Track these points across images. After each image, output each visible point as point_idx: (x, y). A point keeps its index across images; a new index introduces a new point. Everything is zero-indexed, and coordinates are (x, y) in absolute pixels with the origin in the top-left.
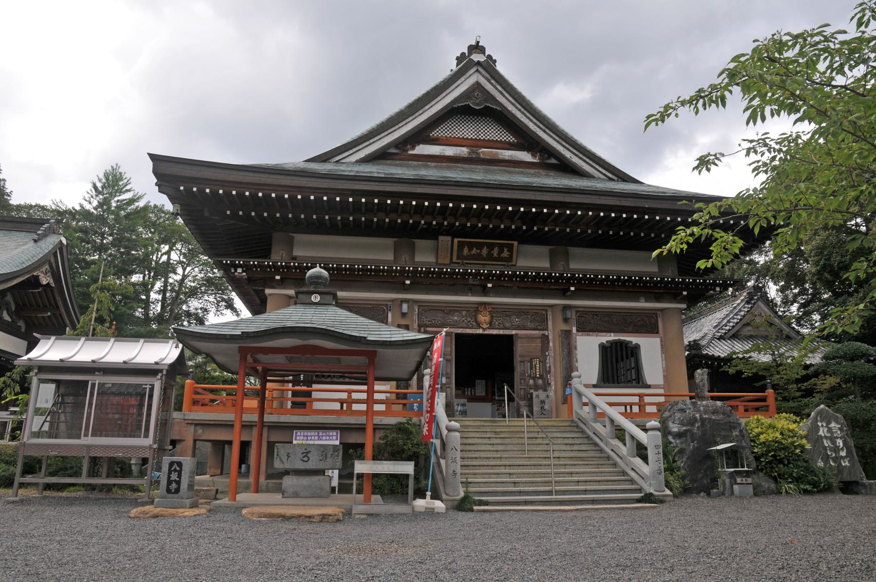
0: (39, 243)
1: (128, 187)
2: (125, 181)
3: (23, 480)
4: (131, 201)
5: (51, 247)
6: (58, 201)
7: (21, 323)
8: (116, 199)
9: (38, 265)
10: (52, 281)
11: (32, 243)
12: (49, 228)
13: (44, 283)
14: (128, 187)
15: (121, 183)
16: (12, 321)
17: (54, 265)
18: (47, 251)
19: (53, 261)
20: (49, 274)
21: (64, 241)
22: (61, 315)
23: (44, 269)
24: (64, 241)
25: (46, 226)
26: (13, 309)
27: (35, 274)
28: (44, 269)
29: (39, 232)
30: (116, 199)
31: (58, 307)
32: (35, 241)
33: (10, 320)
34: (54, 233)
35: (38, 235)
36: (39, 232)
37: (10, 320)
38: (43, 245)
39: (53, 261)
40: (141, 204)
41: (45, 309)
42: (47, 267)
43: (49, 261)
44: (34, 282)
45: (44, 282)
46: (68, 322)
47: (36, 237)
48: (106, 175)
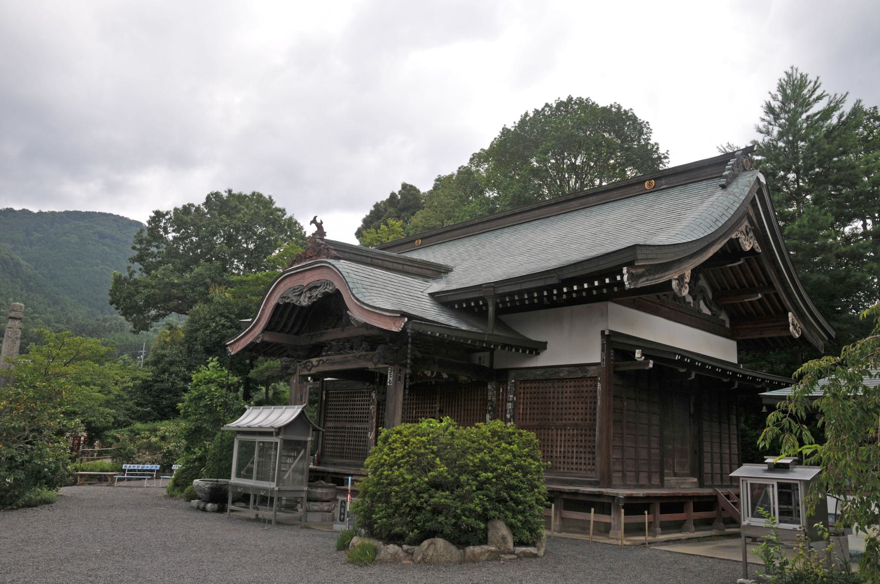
0: (730, 189)
1: (818, 93)
2: (812, 84)
3: (233, 507)
4: (827, 114)
5: (747, 189)
6: (725, 145)
7: (723, 316)
8: (804, 116)
9: (733, 224)
10: (757, 245)
11: (719, 193)
12: (737, 164)
13: (748, 249)
14: (818, 93)
15: (805, 92)
16: (713, 315)
17: (754, 219)
18: (743, 198)
19: (752, 213)
20: (751, 234)
21: (763, 180)
22: (777, 295)
23: (743, 228)
24: (763, 180)
25: (732, 161)
26: (711, 297)
27: (733, 236)
28: (743, 228)
29: (726, 173)
30: (804, 116)
31: (771, 284)
32: (723, 187)
33: (709, 313)
34: (745, 170)
35: (726, 177)
36: (726, 173)
37: (709, 313)
38: (736, 190)
39: (752, 213)
40: (847, 108)
41: (753, 291)
42: (746, 223)
43: (751, 213)
44: (733, 250)
45: (748, 248)
46: (788, 304)
47: (723, 181)
48: (782, 88)
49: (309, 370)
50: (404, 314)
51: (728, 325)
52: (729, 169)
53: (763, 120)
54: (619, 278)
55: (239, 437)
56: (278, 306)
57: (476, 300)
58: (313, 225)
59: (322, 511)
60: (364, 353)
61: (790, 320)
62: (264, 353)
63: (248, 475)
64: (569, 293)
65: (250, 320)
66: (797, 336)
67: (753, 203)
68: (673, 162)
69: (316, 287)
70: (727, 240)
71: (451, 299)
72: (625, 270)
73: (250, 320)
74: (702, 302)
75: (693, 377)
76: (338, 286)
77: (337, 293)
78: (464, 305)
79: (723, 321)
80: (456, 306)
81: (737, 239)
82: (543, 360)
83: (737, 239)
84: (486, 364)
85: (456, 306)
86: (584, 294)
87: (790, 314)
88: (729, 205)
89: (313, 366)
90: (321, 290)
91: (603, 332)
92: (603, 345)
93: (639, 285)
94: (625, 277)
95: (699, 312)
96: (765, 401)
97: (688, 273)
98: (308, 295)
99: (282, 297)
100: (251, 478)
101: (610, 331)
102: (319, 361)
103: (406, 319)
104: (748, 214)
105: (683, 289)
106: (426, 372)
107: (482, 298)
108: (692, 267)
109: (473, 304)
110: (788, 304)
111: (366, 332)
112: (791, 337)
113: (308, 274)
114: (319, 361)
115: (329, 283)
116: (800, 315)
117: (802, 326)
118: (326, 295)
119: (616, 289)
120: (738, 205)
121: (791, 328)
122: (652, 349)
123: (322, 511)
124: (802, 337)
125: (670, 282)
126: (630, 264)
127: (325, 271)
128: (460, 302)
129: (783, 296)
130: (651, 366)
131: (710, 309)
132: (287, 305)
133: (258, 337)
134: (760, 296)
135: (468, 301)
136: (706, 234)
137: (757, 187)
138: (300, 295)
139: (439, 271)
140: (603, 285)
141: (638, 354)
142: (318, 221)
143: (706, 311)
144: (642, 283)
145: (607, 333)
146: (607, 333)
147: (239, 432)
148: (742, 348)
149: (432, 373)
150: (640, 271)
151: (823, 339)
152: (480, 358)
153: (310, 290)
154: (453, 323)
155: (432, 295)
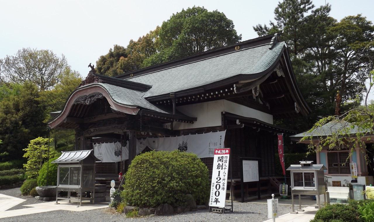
5: (280, 50)
7: (268, 105)
10: (283, 74)
13: (280, 75)
17: (282, 63)
18: (279, 53)
19: (281, 60)
20: (281, 69)
27: (275, 70)
39: (281, 60)
49: (89, 134)
50: (138, 107)
51: (269, 108)
52: (272, 41)
53: (272, 24)
54: (231, 89)
55: (60, 166)
56: (74, 105)
57: (167, 100)
58: (90, 67)
59: (100, 197)
60: (117, 125)
61: (295, 105)
62: (66, 127)
63: (66, 183)
64: (191, 99)
65: (59, 112)
66: (298, 112)
67: (282, 57)
68: (244, 39)
69: (93, 96)
70: (272, 72)
71: (155, 100)
72: (234, 86)
73: (59, 112)
74: (259, 99)
75: (259, 130)
76: (104, 95)
77: (104, 99)
78: (161, 103)
79: (268, 107)
80: (157, 103)
81: (276, 71)
82: (197, 125)
83: (276, 71)
84: (170, 128)
85: (157, 103)
86: (185, 101)
87: (295, 103)
88: (274, 57)
89: (91, 132)
90: (96, 97)
91: (222, 113)
92: (222, 118)
93: (241, 92)
94: (235, 89)
95: (259, 103)
96: (292, 139)
97: (258, 86)
98: (89, 100)
99: (76, 101)
100: (302, 186)
101: (225, 112)
102: (94, 130)
103: (139, 109)
104: (280, 61)
105: (257, 93)
106: (142, 133)
107: (169, 99)
108: (260, 84)
109: (165, 102)
110: (295, 99)
111: (117, 116)
112: (295, 113)
113: (89, 90)
114: (94, 130)
115: (100, 94)
116: (299, 104)
117: (300, 108)
118: (99, 99)
119: (229, 94)
120: (277, 57)
121: (296, 109)
122: (243, 120)
123: (100, 197)
124: (300, 113)
125: (251, 90)
126: (237, 83)
127: (98, 88)
128: (159, 101)
129: (293, 96)
130: (243, 126)
131: (262, 102)
132: (78, 104)
133: (64, 120)
134: (283, 96)
135: (163, 101)
136: (266, 69)
137: (284, 49)
138: (85, 100)
139: (144, 88)
140: (224, 92)
141: (238, 122)
142: (92, 65)
143: (261, 103)
144: (242, 91)
145: (224, 113)
146: (224, 113)
147: (59, 164)
148: (274, 118)
149: (145, 133)
150: (241, 85)
151: (306, 112)
152: (167, 126)
153: (90, 97)
154: (158, 110)
155: (146, 98)
